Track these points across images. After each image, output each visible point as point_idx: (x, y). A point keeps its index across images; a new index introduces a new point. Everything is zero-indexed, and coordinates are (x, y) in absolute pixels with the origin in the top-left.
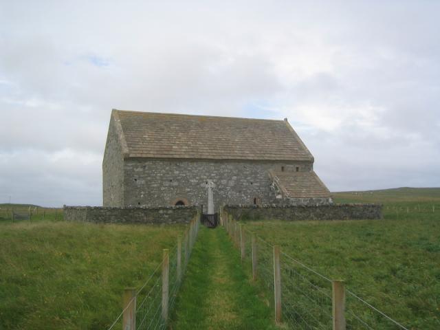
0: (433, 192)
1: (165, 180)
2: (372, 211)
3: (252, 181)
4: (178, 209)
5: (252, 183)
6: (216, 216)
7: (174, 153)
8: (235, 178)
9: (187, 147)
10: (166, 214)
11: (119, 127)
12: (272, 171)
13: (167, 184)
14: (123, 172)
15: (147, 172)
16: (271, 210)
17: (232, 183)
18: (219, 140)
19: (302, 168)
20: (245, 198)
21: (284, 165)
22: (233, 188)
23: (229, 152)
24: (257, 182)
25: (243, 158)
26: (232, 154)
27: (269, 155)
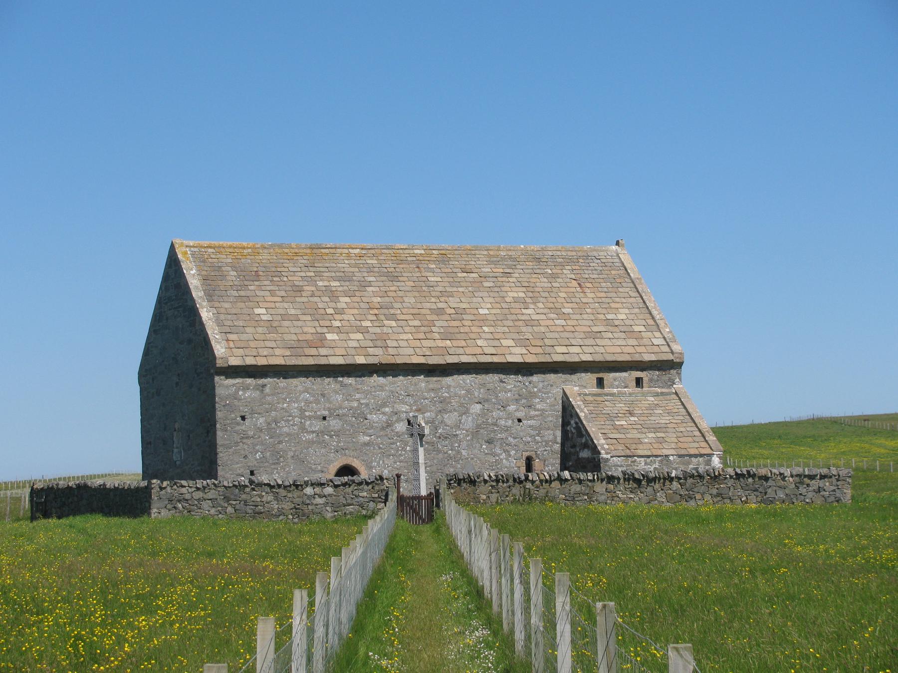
0: (896, 414)
1: (310, 418)
2: (819, 490)
3: (520, 415)
4: (344, 485)
5: (520, 420)
6: (435, 498)
7: (330, 352)
8: (477, 408)
9: (359, 336)
10: (320, 496)
11: (197, 287)
12: (578, 389)
13: (318, 425)
14: (42, 522)
15: (269, 398)
16: (556, 484)
17: (468, 422)
18: (440, 312)
19: (651, 380)
20: (503, 456)
21: (639, 374)
22: (475, 433)
23: (463, 343)
24: (532, 418)
25: (496, 359)
26: (468, 351)
27: (563, 349)
